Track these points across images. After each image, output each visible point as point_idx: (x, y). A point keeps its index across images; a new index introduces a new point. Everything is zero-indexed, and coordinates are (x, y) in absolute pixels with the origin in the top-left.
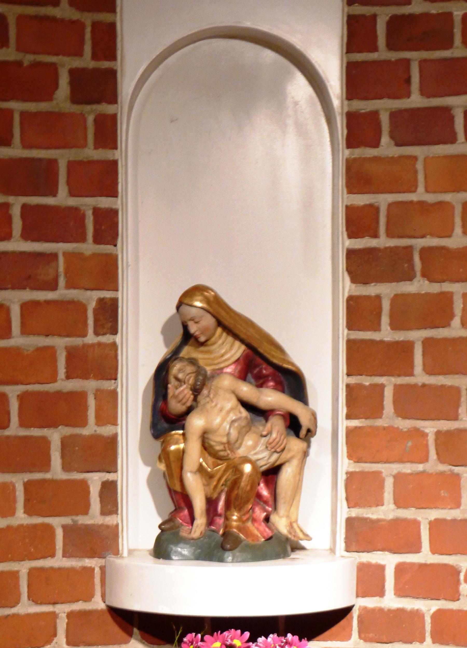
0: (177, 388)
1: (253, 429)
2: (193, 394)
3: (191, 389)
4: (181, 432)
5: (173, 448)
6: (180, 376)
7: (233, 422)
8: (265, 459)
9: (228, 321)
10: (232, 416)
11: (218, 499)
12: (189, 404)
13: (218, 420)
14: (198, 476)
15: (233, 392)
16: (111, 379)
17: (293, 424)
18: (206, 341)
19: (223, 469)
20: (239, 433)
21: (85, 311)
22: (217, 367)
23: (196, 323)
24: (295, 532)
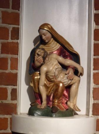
0: (37, 57)
1: (63, 72)
2: (43, 59)
3: (43, 58)
4: (39, 72)
5: (39, 72)
6: (39, 53)
7: (56, 69)
8: (67, 82)
9: (55, 36)
10: (56, 67)
11: (50, 96)
12: (42, 63)
13: (51, 68)
14: (44, 87)
15: (57, 59)
16: (16, 54)
17: (76, 72)
18: (48, 42)
19: (52, 85)
20: (58, 73)
21: (8, 31)
22: (51, 51)
23: (45, 35)
24: (76, 108)
